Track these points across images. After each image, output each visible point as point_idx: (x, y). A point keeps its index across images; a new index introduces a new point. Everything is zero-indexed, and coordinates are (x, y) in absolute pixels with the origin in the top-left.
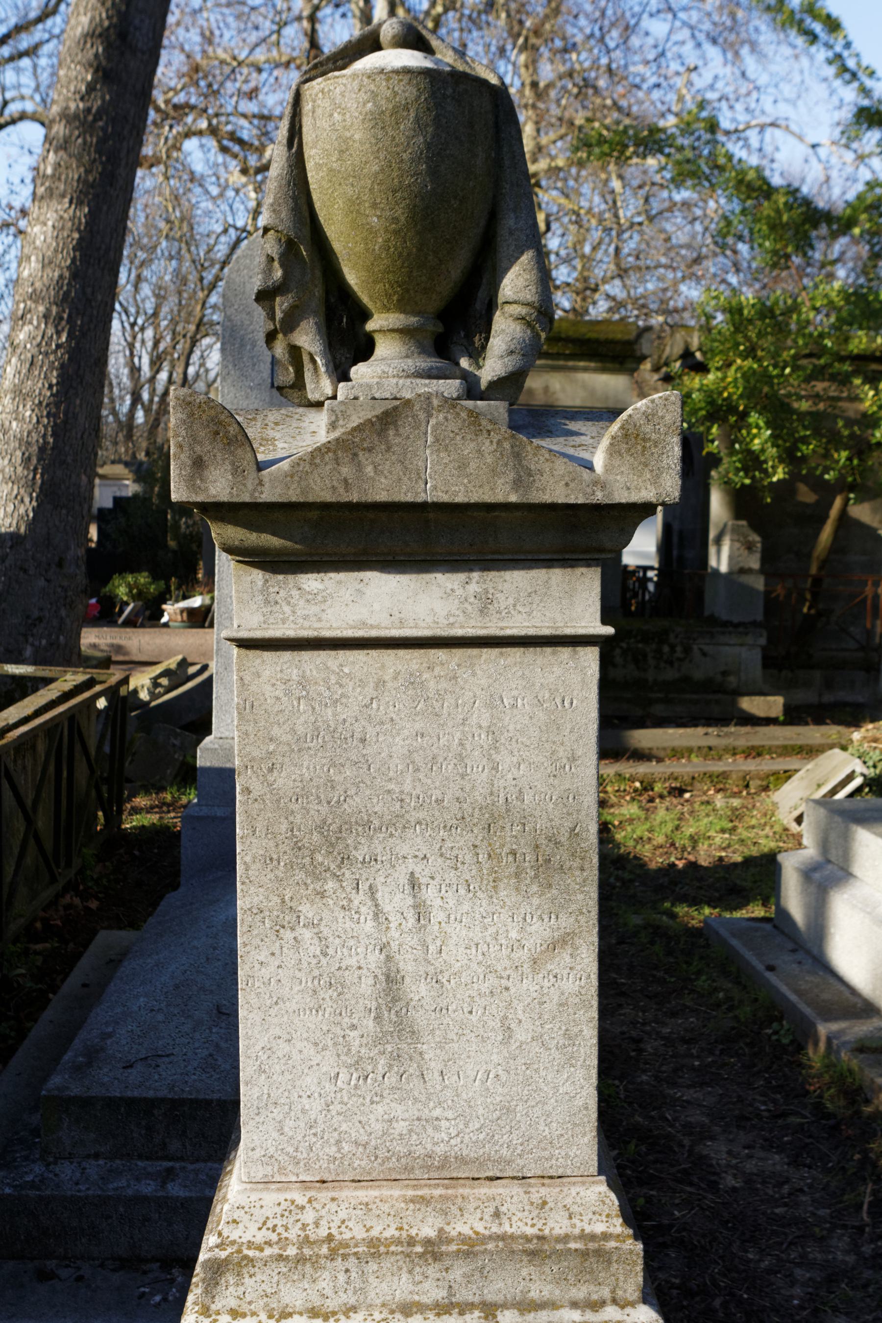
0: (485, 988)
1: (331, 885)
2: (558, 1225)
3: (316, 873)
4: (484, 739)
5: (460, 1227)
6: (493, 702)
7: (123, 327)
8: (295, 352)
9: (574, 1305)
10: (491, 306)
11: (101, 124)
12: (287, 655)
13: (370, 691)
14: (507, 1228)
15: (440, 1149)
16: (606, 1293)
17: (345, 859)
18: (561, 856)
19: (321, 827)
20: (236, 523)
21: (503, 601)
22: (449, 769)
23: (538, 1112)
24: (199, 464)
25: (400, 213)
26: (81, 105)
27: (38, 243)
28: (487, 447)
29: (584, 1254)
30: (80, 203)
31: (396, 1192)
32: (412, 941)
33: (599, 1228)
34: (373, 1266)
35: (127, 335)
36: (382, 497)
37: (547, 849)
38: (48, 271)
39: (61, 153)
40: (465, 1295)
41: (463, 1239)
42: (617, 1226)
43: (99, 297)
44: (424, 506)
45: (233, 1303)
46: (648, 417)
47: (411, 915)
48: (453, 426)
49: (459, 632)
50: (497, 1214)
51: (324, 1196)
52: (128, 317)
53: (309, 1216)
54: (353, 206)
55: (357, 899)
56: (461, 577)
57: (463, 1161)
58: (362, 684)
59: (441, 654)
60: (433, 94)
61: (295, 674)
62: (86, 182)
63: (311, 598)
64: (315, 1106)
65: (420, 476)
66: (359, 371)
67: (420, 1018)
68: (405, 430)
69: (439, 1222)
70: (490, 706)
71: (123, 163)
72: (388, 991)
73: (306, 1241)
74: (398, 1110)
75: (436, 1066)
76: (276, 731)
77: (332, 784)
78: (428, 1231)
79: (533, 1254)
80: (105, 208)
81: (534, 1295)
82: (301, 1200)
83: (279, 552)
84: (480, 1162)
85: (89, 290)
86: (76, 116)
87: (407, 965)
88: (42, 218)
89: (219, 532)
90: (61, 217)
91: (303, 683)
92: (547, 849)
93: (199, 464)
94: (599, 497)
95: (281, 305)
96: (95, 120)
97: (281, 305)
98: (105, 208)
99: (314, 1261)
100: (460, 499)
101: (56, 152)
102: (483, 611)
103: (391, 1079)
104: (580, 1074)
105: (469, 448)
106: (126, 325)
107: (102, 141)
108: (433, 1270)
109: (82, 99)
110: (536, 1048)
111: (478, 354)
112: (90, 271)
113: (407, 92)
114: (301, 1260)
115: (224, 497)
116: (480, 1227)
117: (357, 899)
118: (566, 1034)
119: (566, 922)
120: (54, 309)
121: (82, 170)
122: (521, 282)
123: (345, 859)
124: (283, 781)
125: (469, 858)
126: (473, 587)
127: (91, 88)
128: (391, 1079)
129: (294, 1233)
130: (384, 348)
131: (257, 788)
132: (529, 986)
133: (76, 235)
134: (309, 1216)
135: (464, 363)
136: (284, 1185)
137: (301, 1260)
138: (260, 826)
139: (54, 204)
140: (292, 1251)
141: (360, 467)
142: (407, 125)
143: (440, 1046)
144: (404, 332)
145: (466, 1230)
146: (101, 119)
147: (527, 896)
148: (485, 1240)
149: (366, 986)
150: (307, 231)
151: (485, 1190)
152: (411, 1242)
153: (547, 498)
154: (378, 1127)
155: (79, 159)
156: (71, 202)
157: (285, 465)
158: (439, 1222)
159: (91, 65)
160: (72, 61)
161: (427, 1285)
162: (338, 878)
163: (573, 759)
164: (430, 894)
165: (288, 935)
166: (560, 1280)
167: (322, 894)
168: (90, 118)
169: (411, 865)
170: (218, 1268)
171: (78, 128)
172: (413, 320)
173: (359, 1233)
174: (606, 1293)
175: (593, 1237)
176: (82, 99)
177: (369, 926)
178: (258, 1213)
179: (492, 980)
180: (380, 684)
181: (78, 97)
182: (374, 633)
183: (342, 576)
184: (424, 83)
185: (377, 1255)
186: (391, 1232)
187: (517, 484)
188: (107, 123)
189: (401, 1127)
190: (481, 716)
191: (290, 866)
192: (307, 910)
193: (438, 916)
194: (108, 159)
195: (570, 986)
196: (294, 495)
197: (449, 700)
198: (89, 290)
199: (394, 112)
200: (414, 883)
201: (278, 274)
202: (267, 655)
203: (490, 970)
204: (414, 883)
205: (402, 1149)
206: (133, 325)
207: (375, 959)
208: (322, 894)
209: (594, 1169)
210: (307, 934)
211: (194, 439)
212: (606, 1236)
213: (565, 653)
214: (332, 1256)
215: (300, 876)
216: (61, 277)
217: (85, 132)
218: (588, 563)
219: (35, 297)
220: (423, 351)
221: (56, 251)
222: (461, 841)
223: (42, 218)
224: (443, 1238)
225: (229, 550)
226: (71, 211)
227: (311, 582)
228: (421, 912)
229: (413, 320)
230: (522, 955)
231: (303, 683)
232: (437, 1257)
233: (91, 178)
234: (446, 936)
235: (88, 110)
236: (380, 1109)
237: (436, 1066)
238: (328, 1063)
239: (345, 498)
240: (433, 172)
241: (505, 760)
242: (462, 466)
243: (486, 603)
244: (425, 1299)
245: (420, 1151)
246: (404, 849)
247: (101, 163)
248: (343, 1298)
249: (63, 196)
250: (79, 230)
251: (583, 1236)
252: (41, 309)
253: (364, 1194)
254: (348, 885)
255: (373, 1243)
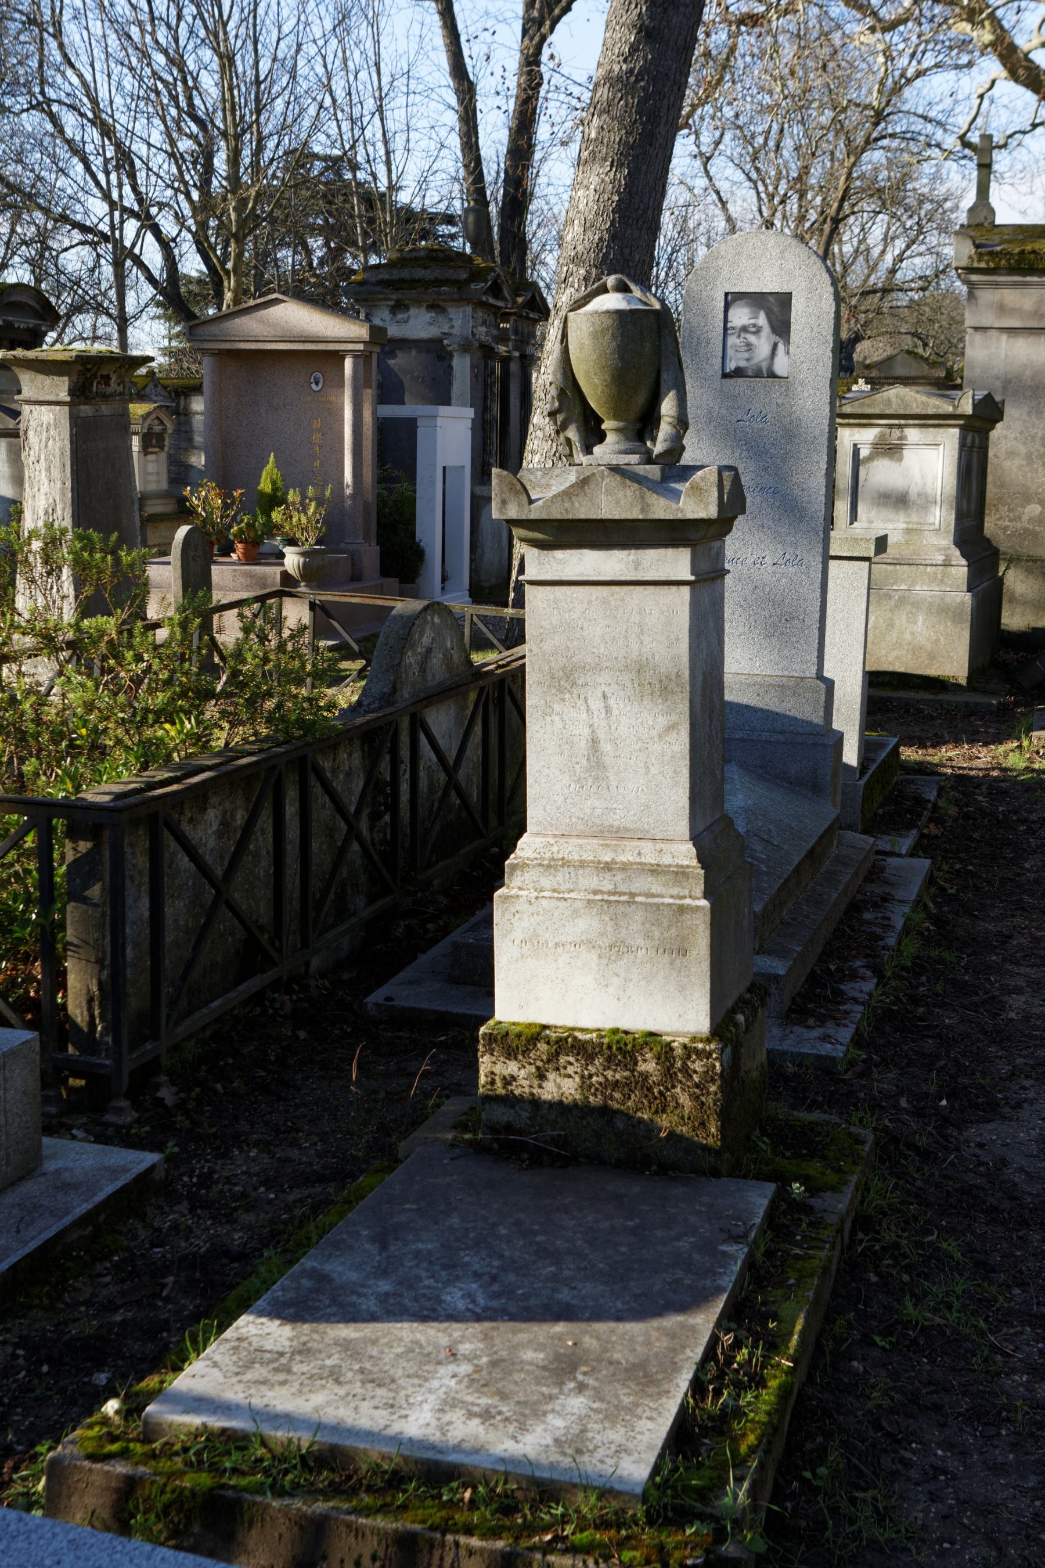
0: (637, 747)
1: (567, 696)
2: (667, 860)
3: (561, 690)
4: (637, 629)
5: (622, 858)
6: (641, 612)
7: (759, 199)
8: (568, 441)
9: (672, 897)
10: (659, 419)
11: (642, 84)
12: (548, 588)
13: (585, 605)
14: (643, 860)
15: (616, 823)
16: (686, 892)
17: (574, 684)
18: (672, 685)
19: (563, 668)
20: (523, 528)
21: (645, 564)
22: (621, 642)
23: (661, 808)
24: (504, 502)
25: (607, 377)
26: (624, 67)
27: (581, 206)
28: (629, 493)
29: (677, 873)
30: (621, 165)
31: (595, 841)
32: (604, 723)
33: (686, 863)
34: (581, 872)
35: (764, 209)
36: (582, 516)
37: (665, 682)
38: (589, 234)
39: (605, 116)
40: (622, 888)
41: (623, 863)
42: (694, 862)
43: (637, 257)
44: (602, 521)
45: (520, 884)
46: (702, 479)
47: (603, 711)
48: (613, 484)
49: (623, 578)
50: (639, 854)
51: (562, 841)
52: (766, 186)
53: (555, 849)
54: (587, 372)
55: (579, 703)
56: (626, 552)
57: (626, 829)
58: (582, 602)
59: (617, 589)
60: (620, 322)
61: (552, 597)
62: (627, 143)
63: (559, 562)
64: (560, 800)
65: (599, 507)
66: (597, 449)
67: (607, 760)
68: (592, 486)
69: (613, 855)
70: (639, 613)
71: (663, 121)
72: (593, 747)
73: (553, 859)
74: (597, 803)
75: (614, 783)
76: (543, 623)
77: (568, 648)
78: (608, 859)
79: (653, 871)
80: (644, 168)
81: (653, 891)
82: (552, 841)
83: (543, 541)
84: (635, 831)
85: (627, 251)
86: (619, 78)
87: (601, 734)
88: (585, 182)
89: (516, 532)
90: (603, 181)
91: (556, 601)
92: (665, 682)
93: (504, 502)
94: (680, 516)
95: (560, 418)
96: (637, 81)
97: (560, 418)
98: (644, 168)
99: (555, 867)
100: (617, 517)
101: (599, 116)
102: (636, 569)
103: (594, 789)
104: (681, 791)
105: (620, 494)
106: (763, 195)
107: (643, 102)
108: (608, 875)
109: (625, 61)
110: (660, 777)
111: (654, 440)
112: (629, 232)
113: (608, 321)
114: (549, 866)
115: (515, 517)
116: (631, 859)
117: (579, 703)
118: (675, 771)
119: (674, 717)
120: (594, 271)
121: (623, 132)
122: (669, 406)
123: (574, 684)
124: (547, 646)
125: (630, 685)
126: (632, 557)
127: (634, 49)
128: (594, 789)
129: (548, 855)
130: (610, 438)
131: (535, 650)
132: (657, 748)
133: (616, 198)
134: (555, 849)
135: (649, 444)
136: (546, 835)
137: (549, 866)
138: (536, 667)
139: (597, 168)
140: (546, 862)
141: (572, 503)
142: (609, 336)
143: (616, 774)
144: (618, 430)
145: (624, 859)
146: (643, 79)
147: (656, 704)
148: (632, 864)
149: (583, 744)
150: (570, 383)
151: (635, 843)
152: (599, 862)
153: (656, 517)
154: (588, 811)
155: (621, 120)
156: (612, 166)
157: (540, 503)
158: (613, 855)
159: (634, 26)
160: (617, 23)
161: (605, 882)
162: (571, 693)
163: (678, 639)
164: (612, 702)
165: (548, 718)
166: (665, 884)
167: (563, 700)
168: (633, 79)
169: (603, 688)
170: (514, 867)
171: (620, 90)
172: (621, 424)
173: (576, 857)
174: (686, 892)
175: (682, 866)
176: (625, 61)
177: (584, 716)
178: (533, 847)
179: (640, 743)
180: (590, 602)
181: (621, 58)
182: (585, 578)
183: (573, 552)
184: (616, 316)
185: (582, 867)
186: (591, 858)
187: (643, 510)
188: (648, 83)
189: (598, 812)
190: (635, 618)
191: (550, 686)
192: (556, 707)
193: (615, 712)
194: (648, 119)
195: (676, 748)
196: (544, 516)
197: (621, 611)
198: (627, 251)
199: (602, 331)
200: (605, 696)
201: (557, 404)
202: (540, 588)
203: (639, 739)
204: (605, 696)
205: (598, 822)
206: (771, 197)
207: (587, 731)
208: (563, 700)
209: (687, 837)
210: (557, 719)
211: (502, 491)
212: (688, 867)
213: (674, 588)
214: (563, 866)
215: (554, 691)
216: (601, 239)
217: (627, 94)
218: (685, 546)
219: (576, 260)
220: (628, 439)
221: (597, 214)
222: (626, 677)
223: (585, 182)
224: (614, 862)
225: (521, 540)
226: (612, 174)
227: (559, 554)
228: (608, 710)
229: (621, 424)
230: (654, 733)
231: (556, 601)
232: (610, 869)
233: (631, 140)
234: (619, 722)
235: (631, 71)
236: (589, 802)
237: (614, 783)
238: (566, 780)
239: (566, 517)
240: (622, 358)
241: (646, 639)
242: (618, 502)
243: (637, 565)
244: (605, 889)
245: (607, 824)
246: (600, 680)
247: (642, 123)
248: (568, 885)
249: (605, 160)
250: (619, 193)
251: (677, 866)
252: (582, 271)
253: (580, 841)
254: (575, 696)
255: (581, 862)
